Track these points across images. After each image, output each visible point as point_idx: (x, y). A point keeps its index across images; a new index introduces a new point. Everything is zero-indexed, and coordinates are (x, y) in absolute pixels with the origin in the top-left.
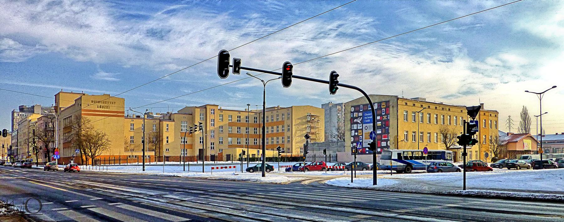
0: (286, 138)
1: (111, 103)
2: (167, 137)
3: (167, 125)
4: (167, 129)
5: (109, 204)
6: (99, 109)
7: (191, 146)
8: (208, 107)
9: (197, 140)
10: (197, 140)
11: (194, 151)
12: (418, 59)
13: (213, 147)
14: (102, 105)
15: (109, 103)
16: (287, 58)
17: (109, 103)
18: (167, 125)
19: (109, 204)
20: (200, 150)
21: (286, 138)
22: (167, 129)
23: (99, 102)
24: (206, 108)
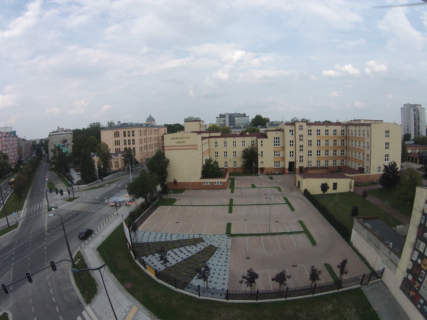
0: (366, 155)
1: (186, 138)
2: (262, 152)
3: (262, 142)
4: (262, 145)
5: (131, 246)
6: (177, 144)
7: (283, 159)
8: (296, 124)
9: (287, 154)
10: (287, 154)
11: (284, 164)
12: (83, 304)
13: (302, 160)
14: (179, 140)
15: (185, 138)
16: (57, 195)
17: (185, 138)
18: (262, 142)
19: (131, 246)
20: (290, 163)
21: (366, 155)
22: (262, 145)
23: (177, 138)
24: (295, 125)
